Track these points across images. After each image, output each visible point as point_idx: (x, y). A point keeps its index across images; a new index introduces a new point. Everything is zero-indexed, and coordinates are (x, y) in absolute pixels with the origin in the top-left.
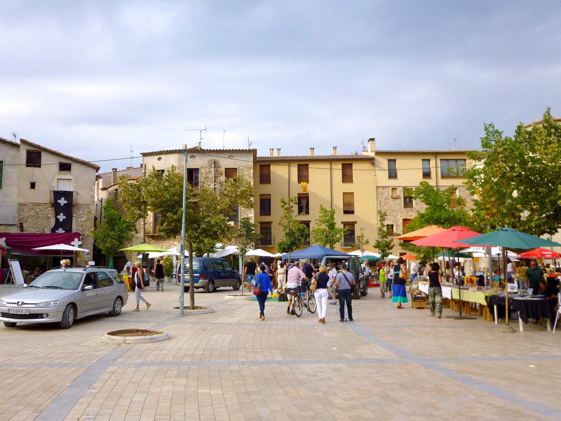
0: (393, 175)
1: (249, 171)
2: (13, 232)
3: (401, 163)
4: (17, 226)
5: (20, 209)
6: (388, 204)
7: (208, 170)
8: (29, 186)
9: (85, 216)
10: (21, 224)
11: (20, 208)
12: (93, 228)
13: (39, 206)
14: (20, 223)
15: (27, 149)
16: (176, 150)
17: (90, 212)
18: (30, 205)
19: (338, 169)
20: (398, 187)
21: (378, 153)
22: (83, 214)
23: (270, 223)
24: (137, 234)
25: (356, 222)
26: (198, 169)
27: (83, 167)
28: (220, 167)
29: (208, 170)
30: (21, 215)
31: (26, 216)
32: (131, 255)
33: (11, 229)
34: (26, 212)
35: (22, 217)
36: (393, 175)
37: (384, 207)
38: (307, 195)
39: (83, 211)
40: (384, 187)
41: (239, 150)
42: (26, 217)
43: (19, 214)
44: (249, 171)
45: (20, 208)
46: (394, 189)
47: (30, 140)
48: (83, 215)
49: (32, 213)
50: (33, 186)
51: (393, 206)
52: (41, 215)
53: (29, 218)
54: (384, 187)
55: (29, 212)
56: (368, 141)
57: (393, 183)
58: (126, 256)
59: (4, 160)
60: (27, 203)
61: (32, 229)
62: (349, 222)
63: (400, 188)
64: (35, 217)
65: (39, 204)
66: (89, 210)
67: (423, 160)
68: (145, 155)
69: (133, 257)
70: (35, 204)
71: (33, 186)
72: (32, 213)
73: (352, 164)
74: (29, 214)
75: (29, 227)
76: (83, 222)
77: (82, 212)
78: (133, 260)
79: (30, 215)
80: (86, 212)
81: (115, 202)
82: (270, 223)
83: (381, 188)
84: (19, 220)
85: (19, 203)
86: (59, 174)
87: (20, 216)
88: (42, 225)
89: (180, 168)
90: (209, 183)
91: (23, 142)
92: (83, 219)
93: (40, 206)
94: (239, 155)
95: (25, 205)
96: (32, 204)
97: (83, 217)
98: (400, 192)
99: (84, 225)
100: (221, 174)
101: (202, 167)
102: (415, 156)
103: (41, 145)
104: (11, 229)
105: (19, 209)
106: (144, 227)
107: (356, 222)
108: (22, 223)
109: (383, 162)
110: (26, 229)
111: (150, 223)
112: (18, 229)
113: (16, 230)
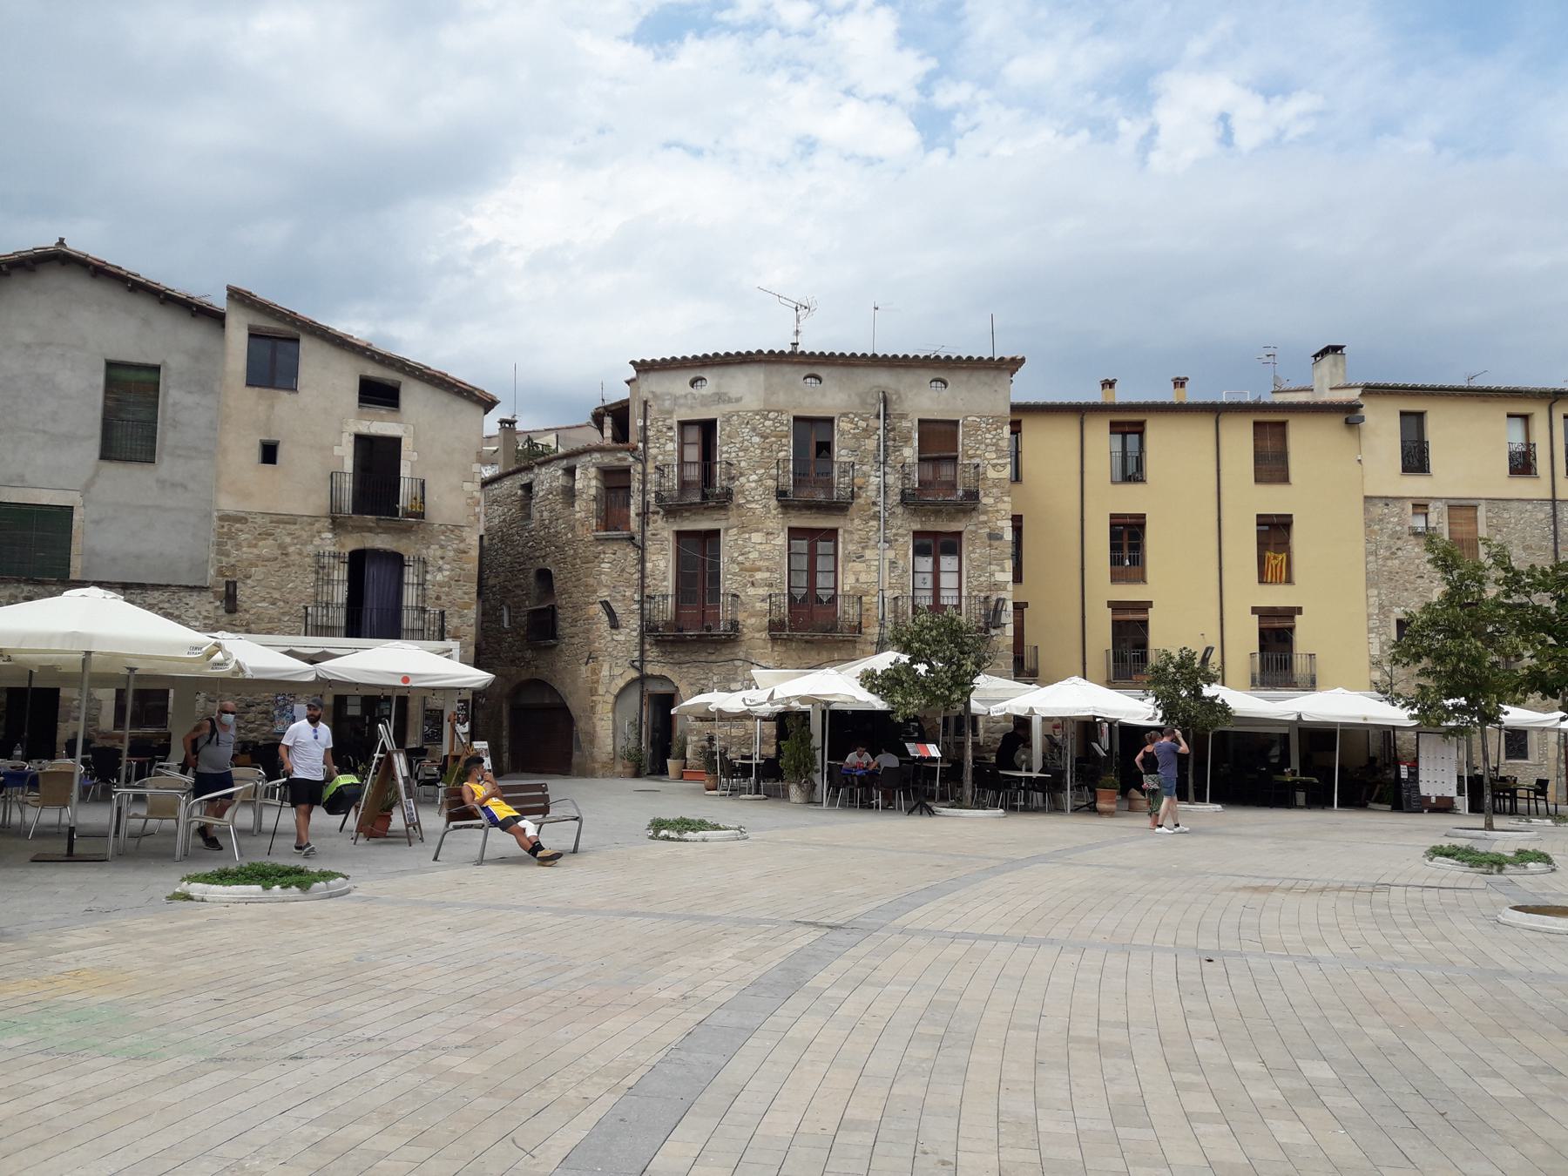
0: (1415, 459)
1: (996, 430)
2: (410, 444)
3: (1441, 426)
4: (215, 593)
5: (223, 534)
6: (1400, 553)
7: (863, 424)
8: (256, 453)
9: (448, 567)
10: (231, 587)
11: (225, 530)
12: (475, 607)
13: (288, 526)
14: (227, 583)
15: (251, 323)
16: (760, 352)
17: (465, 552)
18: (259, 520)
19: (1240, 440)
20: (1432, 498)
21: (1371, 390)
22: (442, 558)
23: (1144, 606)
24: (613, 631)
25: (1299, 610)
26: (830, 421)
27: (441, 397)
28: (903, 416)
29: (863, 424)
30: (228, 556)
31: (247, 559)
32: (593, 701)
33: (192, 604)
34: (244, 544)
35: (233, 561)
36: (1415, 459)
37: (1389, 563)
38: (1142, 520)
39: (442, 547)
40: (1386, 498)
41: (970, 358)
42: (246, 563)
43: (222, 552)
44: (996, 430)
45: (225, 530)
46: (1421, 507)
47: (263, 293)
48: (441, 562)
49: (266, 548)
50: (269, 453)
51: (1417, 561)
52: (297, 557)
53: (257, 566)
54: (1387, 500)
55: (255, 546)
56: (1316, 356)
57: (1416, 486)
58: (568, 704)
59: (164, 362)
60: (249, 513)
61: (264, 604)
62: (1274, 608)
63: (1439, 504)
64: (276, 565)
65: (291, 520)
66: (462, 546)
67: (1510, 416)
68: (643, 367)
69: (599, 708)
70: (275, 518)
71: (269, 453)
72: (266, 548)
73: (1283, 424)
74: (255, 551)
75: (254, 599)
76: (441, 585)
77: (439, 553)
78: (598, 716)
79: (258, 556)
80: (452, 554)
81: (523, 528)
82: (1144, 606)
83: (1377, 501)
84: (220, 573)
85: (221, 513)
86: (360, 417)
87: (224, 559)
88: (301, 592)
89: (772, 415)
90: (864, 468)
91: (238, 297)
92: (439, 577)
93: (293, 527)
94: (962, 376)
95: (242, 520)
96: (267, 519)
97: (440, 569)
98: (1440, 515)
99: (443, 597)
100: (907, 440)
101: (845, 415)
102: (1484, 401)
103: (299, 313)
104: (192, 604)
105: (220, 535)
106: (642, 608)
107: (1299, 610)
108: (235, 583)
109: (1383, 424)
110: (245, 606)
111: (665, 597)
112: (218, 603)
113: (209, 607)
